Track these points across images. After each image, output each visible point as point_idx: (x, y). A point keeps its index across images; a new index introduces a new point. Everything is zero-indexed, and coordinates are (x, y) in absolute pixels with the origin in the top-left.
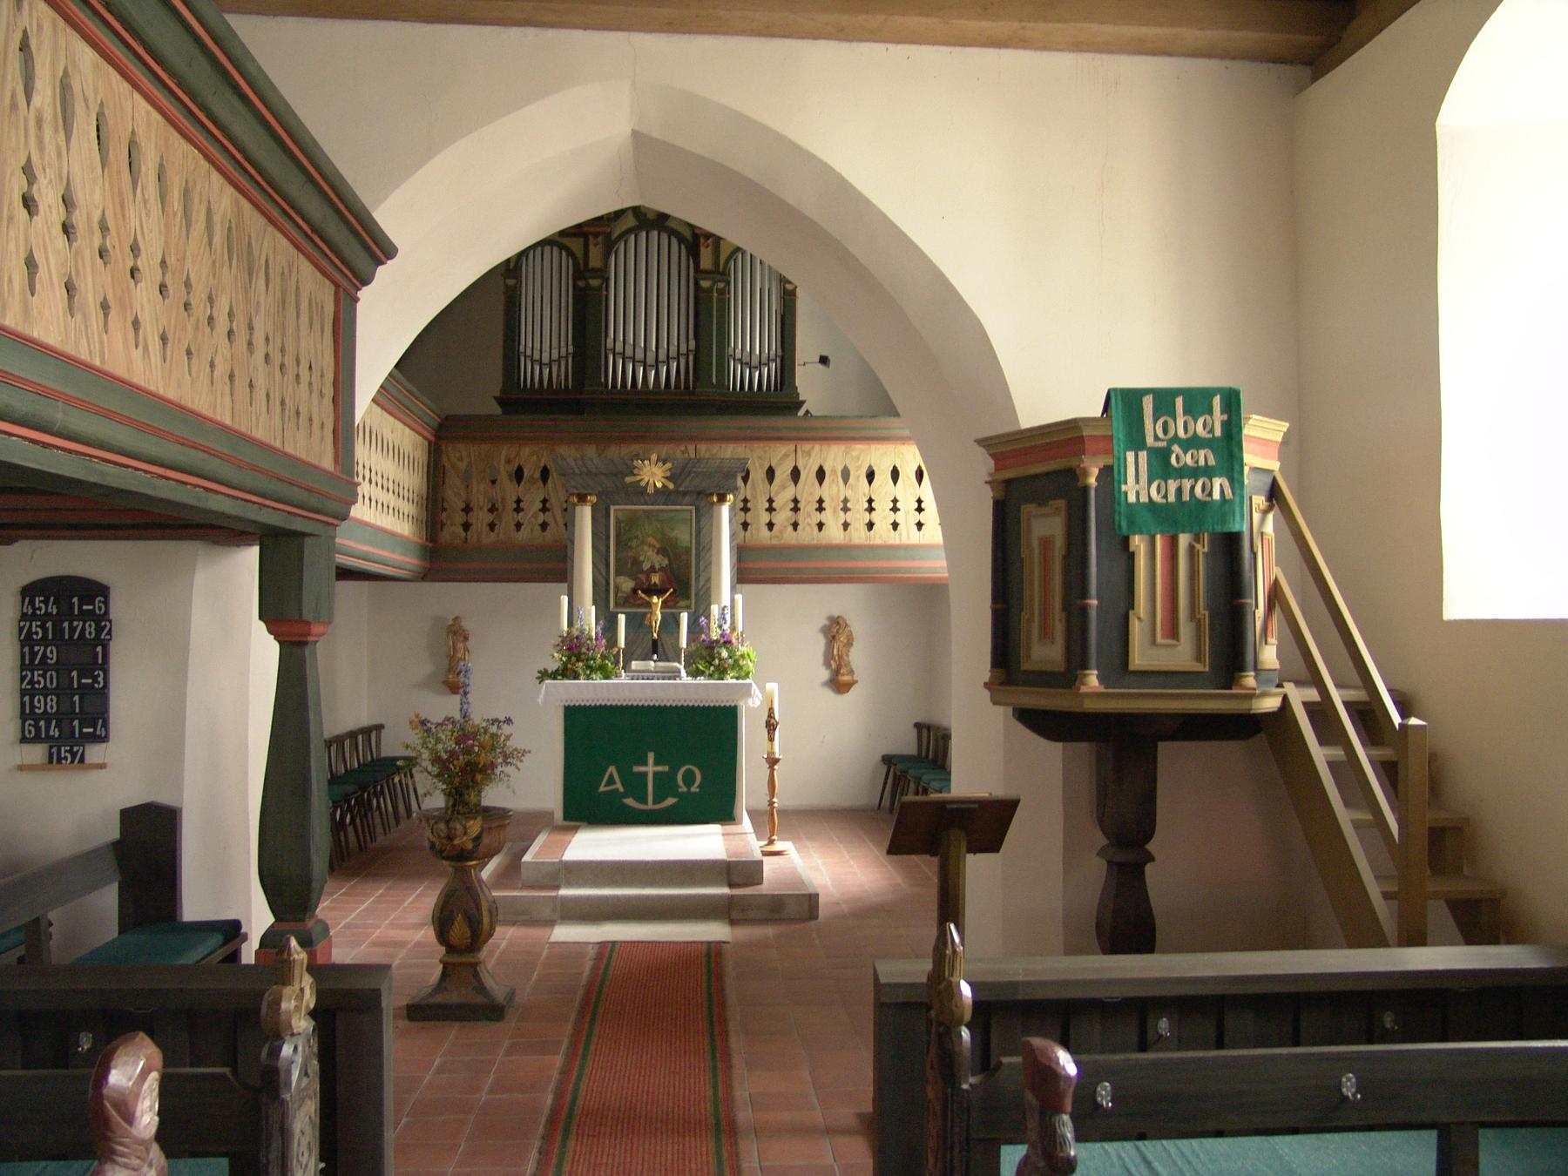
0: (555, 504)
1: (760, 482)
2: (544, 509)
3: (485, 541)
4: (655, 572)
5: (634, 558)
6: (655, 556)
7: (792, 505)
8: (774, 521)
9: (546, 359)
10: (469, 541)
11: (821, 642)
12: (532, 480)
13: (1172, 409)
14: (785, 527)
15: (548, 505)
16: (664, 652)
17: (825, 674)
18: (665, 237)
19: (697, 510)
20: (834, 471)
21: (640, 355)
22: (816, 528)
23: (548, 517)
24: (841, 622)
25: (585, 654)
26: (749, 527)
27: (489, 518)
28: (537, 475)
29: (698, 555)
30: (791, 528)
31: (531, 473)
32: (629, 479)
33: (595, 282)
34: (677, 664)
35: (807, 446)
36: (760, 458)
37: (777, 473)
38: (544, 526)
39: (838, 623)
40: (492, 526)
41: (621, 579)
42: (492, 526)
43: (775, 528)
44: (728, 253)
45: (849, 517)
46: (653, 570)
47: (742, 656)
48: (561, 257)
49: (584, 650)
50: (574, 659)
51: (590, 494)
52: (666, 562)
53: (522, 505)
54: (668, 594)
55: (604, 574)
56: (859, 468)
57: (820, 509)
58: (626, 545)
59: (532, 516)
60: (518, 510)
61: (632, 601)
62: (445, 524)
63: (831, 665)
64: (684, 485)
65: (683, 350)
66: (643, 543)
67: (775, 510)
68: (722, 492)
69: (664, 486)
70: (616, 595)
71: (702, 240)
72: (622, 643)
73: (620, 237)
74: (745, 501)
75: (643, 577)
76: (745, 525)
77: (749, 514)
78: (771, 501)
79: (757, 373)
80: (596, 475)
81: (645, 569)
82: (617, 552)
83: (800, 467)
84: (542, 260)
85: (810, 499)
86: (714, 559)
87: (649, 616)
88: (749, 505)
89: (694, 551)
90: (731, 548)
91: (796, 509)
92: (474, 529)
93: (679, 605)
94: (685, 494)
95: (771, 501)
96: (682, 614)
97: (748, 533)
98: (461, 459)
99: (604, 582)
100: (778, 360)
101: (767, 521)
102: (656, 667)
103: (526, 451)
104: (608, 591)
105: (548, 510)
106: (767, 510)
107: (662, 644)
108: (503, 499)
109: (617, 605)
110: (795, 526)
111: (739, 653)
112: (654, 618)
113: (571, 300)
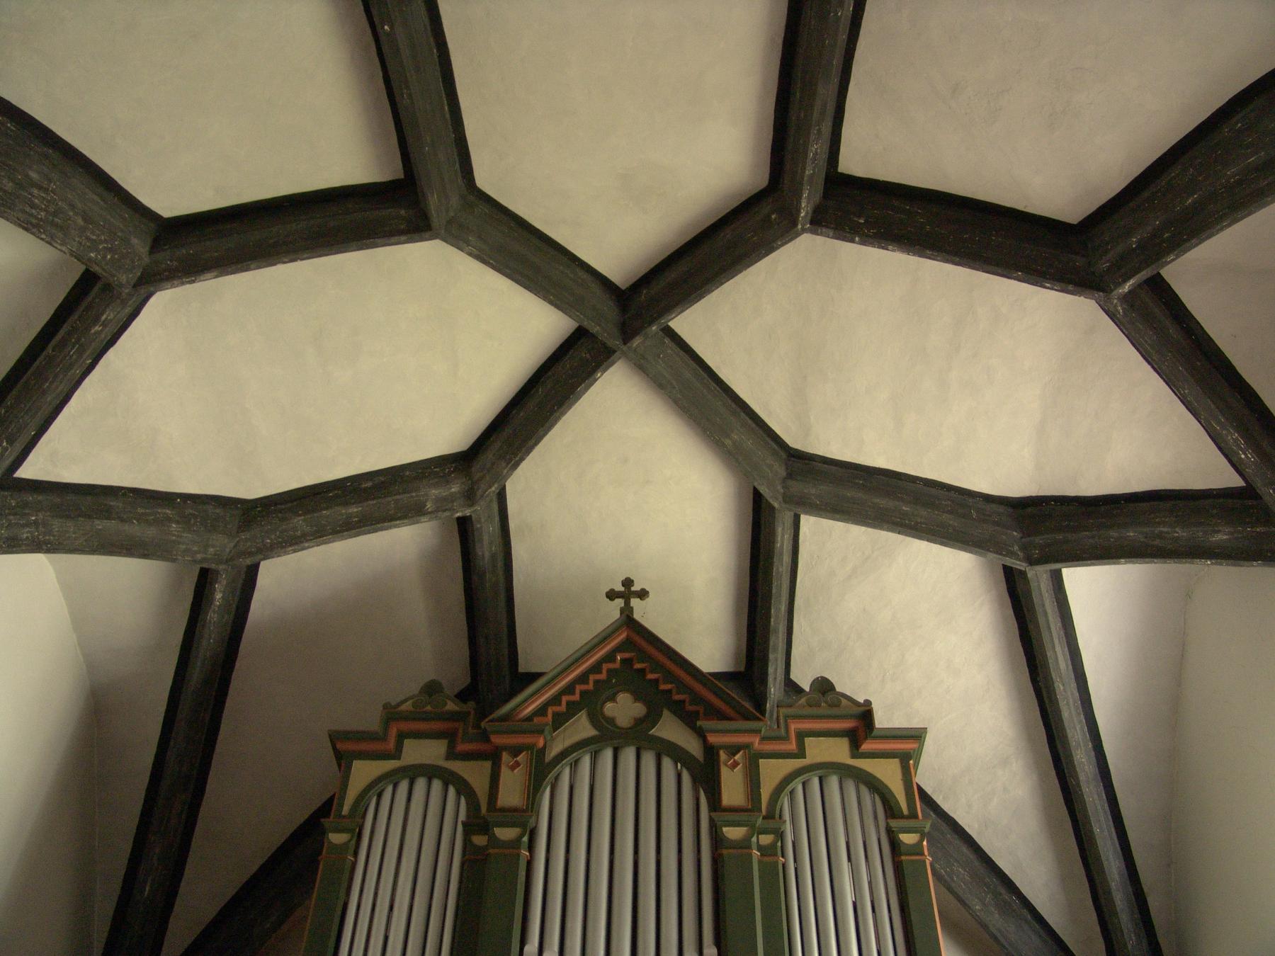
13: (461, 904)
18: (649, 760)
33: (505, 834)
71: (723, 756)
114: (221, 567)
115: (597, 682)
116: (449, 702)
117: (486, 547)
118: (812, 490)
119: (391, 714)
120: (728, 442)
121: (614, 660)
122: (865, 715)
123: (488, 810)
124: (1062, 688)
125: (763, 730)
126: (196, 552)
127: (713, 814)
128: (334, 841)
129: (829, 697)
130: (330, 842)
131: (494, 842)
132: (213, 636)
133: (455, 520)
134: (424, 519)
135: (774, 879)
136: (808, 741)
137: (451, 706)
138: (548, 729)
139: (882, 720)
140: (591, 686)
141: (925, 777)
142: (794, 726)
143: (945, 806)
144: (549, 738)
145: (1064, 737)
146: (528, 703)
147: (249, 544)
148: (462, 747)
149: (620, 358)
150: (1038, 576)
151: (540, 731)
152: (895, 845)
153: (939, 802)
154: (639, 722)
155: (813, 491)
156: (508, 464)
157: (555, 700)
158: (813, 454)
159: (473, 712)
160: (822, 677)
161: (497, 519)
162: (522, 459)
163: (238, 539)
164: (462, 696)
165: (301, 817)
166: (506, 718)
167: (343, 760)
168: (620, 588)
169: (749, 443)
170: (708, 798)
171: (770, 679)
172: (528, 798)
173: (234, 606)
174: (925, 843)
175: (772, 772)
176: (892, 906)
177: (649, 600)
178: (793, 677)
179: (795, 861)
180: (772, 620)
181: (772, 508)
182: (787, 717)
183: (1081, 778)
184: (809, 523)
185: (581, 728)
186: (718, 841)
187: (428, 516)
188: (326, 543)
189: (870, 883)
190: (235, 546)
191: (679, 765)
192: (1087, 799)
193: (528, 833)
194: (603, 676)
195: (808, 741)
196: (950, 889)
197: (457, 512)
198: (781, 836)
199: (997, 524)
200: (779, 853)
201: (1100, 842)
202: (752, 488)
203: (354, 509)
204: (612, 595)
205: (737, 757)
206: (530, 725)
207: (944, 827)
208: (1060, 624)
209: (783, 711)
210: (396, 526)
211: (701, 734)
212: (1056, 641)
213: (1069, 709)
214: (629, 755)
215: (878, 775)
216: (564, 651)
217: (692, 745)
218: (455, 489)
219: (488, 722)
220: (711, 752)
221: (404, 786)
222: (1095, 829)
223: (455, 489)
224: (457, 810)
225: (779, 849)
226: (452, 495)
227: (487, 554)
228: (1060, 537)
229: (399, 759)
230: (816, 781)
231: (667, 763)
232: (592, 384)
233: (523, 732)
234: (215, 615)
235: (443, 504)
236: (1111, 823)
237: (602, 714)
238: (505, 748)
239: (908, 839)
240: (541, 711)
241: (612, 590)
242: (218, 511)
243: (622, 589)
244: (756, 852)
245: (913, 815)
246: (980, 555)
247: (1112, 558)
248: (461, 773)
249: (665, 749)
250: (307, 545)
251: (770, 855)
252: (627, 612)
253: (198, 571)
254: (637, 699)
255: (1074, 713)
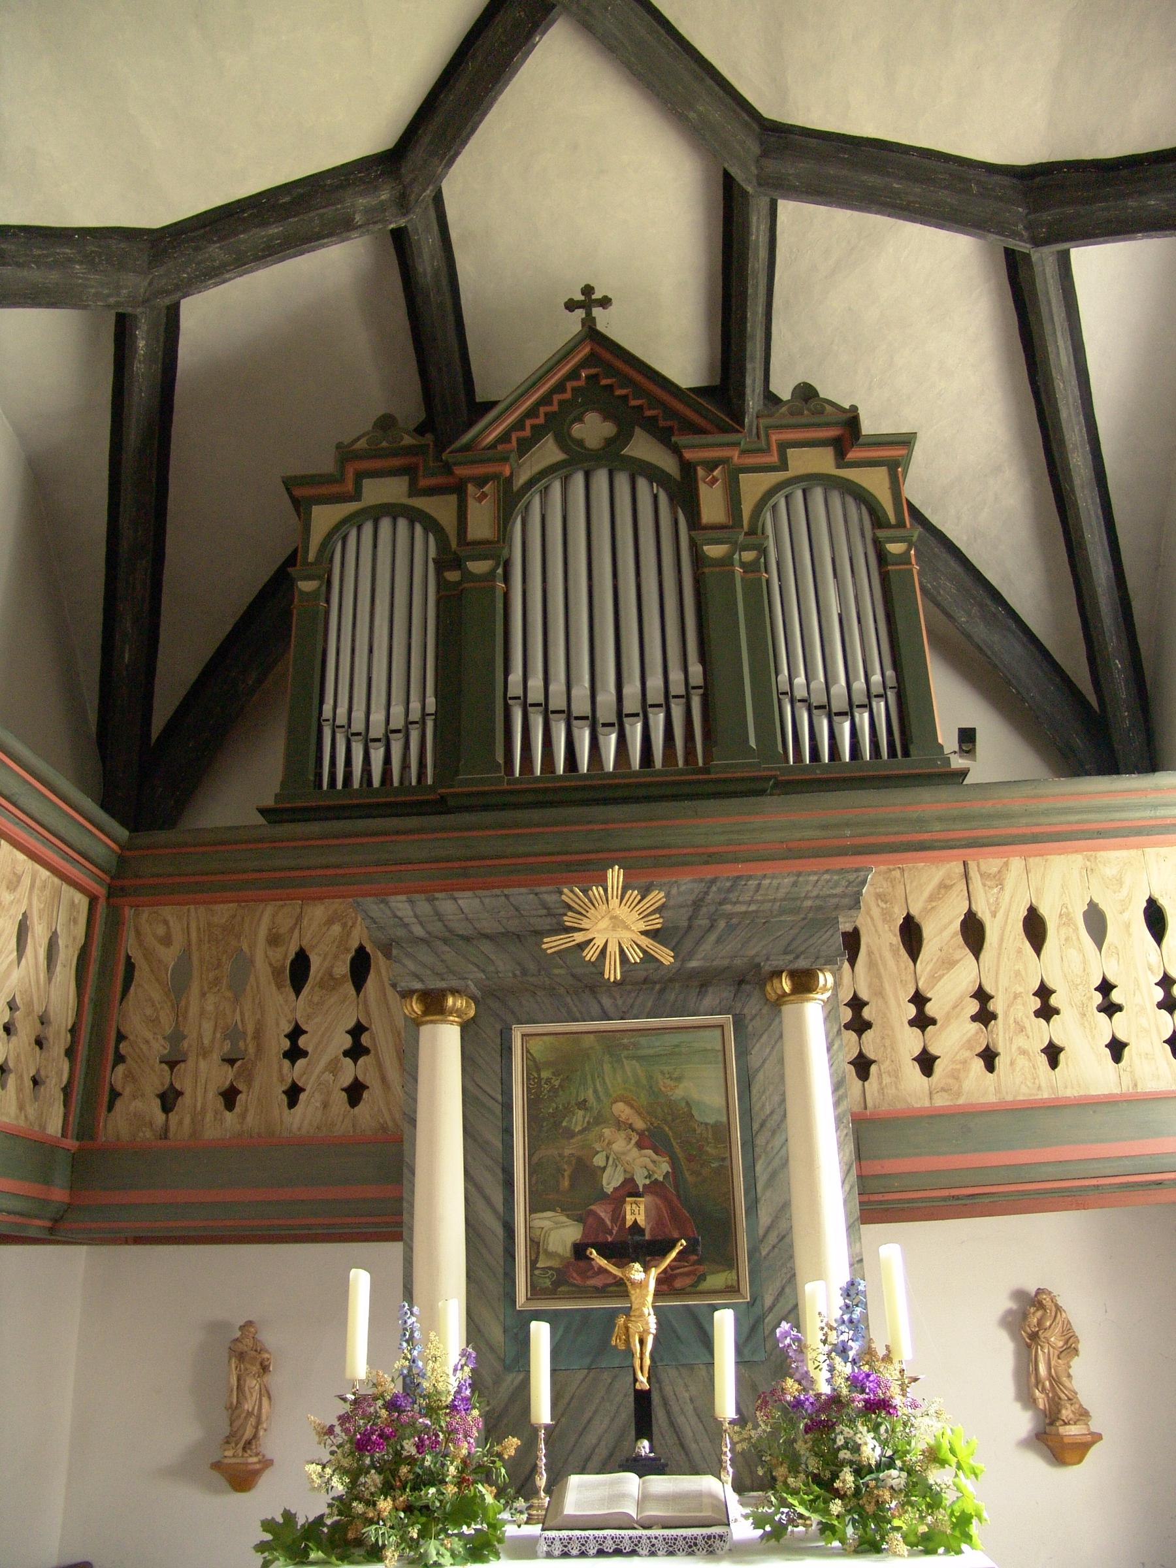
0: (380, 1038)
1: (888, 955)
2: (356, 1052)
3: (211, 1132)
4: (637, 1194)
5: (580, 1160)
6: (635, 1152)
7: (974, 1007)
8: (933, 1050)
9: (377, 731)
10: (171, 1135)
11: (1004, 1349)
12: (329, 983)
14: (964, 1062)
15: (365, 1040)
16: (672, 1424)
17: (1023, 1422)
18: (622, 482)
19: (739, 1024)
20: (1066, 918)
21: (581, 706)
22: (1043, 1059)
23: (364, 1069)
24: (1047, 1301)
25: (411, 1461)
26: (873, 1068)
27: (226, 1076)
28: (343, 968)
29: (749, 1144)
30: (980, 1063)
31: (326, 964)
32: (553, 944)
33: (478, 567)
34: (707, 1483)
35: (990, 863)
36: (880, 897)
37: (927, 932)
38: (355, 1092)
39: (1040, 1305)
40: (230, 1097)
41: (545, 1220)
42: (230, 1097)
43: (939, 1067)
44: (759, 495)
45: (1121, 1026)
46: (630, 1189)
47: (933, 1456)
48: (413, 538)
49: (409, 1447)
50: (373, 1480)
51: (455, 992)
52: (665, 1167)
53: (302, 1042)
54: (674, 1254)
55: (500, 1207)
56: (1124, 907)
57: (1047, 1012)
58: (557, 1125)
59: (326, 1069)
60: (294, 1053)
61: (578, 1280)
62: (120, 1094)
63: (1035, 1401)
64: (701, 954)
65: (677, 687)
66: (599, 1120)
67: (933, 1022)
68: (802, 964)
69: (648, 957)
70: (533, 1264)
71: (701, 472)
72: (542, 1411)
73: (531, 483)
74: (857, 1004)
75: (603, 1212)
76: (862, 1065)
77: (868, 1035)
78: (919, 1000)
79: (847, 726)
80: (467, 939)
81: (609, 1189)
82: (532, 1147)
83: (983, 912)
84: (375, 546)
85: (1020, 989)
86: (795, 1149)
87: (621, 1320)
88: (866, 1013)
89: (737, 1135)
90: (839, 1120)
91: (985, 1017)
92: (185, 1102)
93: (704, 1286)
94: (703, 981)
95: (919, 1000)
96: (718, 1315)
97: (872, 1084)
98: (167, 941)
99: (500, 1231)
100: (891, 695)
101: (917, 1052)
102: (644, 1500)
103: (318, 912)
104: (510, 1254)
105: (366, 1051)
106: (912, 1023)
107: (665, 1403)
108: (258, 1035)
109: (535, 1291)
110: (989, 1057)
111: (919, 1445)
112: (636, 1328)
113: (559, 937)
114: (139, 310)
115: (561, 403)
116: (406, 436)
117: (427, 262)
118: (791, 169)
119: (346, 454)
120: (692, 115)
121: (578, 378)
122: (851, 421)
123: (459, 545)
124: (1062, 385)
125: (742, 443)
126: (109, 296)
127: (693, 533)
128: (303, 589)
129: (812, 404)
130: (301, 592)
131: (468, 576)
132: (144, 388)
133: (389, 233)
134: (354, 234)
135: (758, 595)
136: (790, 451)
137: (408, 440)
138: (513, 456)
139: (868, 427)
140: (555, 408)
141: (912, 491)
142: (775, 437)
143: (935, 520)
144: (515, 465)
145: (1062, 442)
146: (488, 430)
147: (164, 281)
148: (423, 483)
149: (559, 15)
150: (1043, 258)
151: (505, 459)
152: (882, 557)
153: (927, 515)
154: (609, 442)
155: (791, 171)
156: (441, 160)
157: (519, 425)
158: (791, 125)
159: (432, 444)
160: (804, 383)
161: (435, 228)
162: (457, 154)
163: (151, 276)
164: (421, 430)
165: (265, 575)
166: (467, 448)
167: (301, 507)
168: (579, 297)
169: (716, 116)
170: (685, 515)
171: (748, 391)
172: (499, 531)
173: (160, 353)
174: (912, 552)
175: (753, 486)
176: (878, 617)
177: (612, 309)
178: (772, 388)
179: (780, 580)
180: (749, 325)
181: (745, 194)
182: (767, 428)
183: (1075, 483)
184: (788, 210)
185: (549, 452)
186: (698, 559)
187: (359, 231)
188: (249, 272)
189: (856, 597)
190: (150, 284)
191: (655, 485)
192: (1080, 505)
193: (502, 563)
194: (568, 395)
195: (790, 451)
196: (938, 605)
197: (391, 223)
198: (764, 552)
199: (1001, 199)
200: (763, 569)
201: (1090, 548)
202: (721, 173)
203: (274, 230)
204: (571, 306)
205: (715, 473)
206: (496, 455)
207: (932, 541)
208: (1063, 315)
209: (763, 422)
210: (323, 246)
211: (676, 450)
212: (1059, 334)
213: (1069, 409)
214: (601, 479)
215: (865, 485)
216: (520, 375)
217: (667, 462)
218: (385, 196)
219: (450, 453)
220: (688, 469)
221: (368, 528)
222: (1086, 534)
223: (385, 196)
224: (425, 547)
225: (762, 566)
226: (382, 203)
227: (429, 270)
228: (1070, 210)
229: (360, 500)
230: (799, 494)
231: (642, 483)
232: (530, 52)
233: (489, 460)
234: (141, 368)
235: (374, 215)
236: (1103, 528)
237: (570, 435)
238: (471, 479)
239: (895, 548)
240: (505, 438)
241: (571, 300)
242: (123, 245)
243: (582, 298)
244: (739, 570)
245: (901, 524)
246: (980, 237)
247: (1128, 232)
248: (427, 510)
249: (640, 469)
250: (228, 276)
251: (753, 572)
252: (589, 324)
253: (114, 318)
254: (605, 419)
255: (1073, 413)
